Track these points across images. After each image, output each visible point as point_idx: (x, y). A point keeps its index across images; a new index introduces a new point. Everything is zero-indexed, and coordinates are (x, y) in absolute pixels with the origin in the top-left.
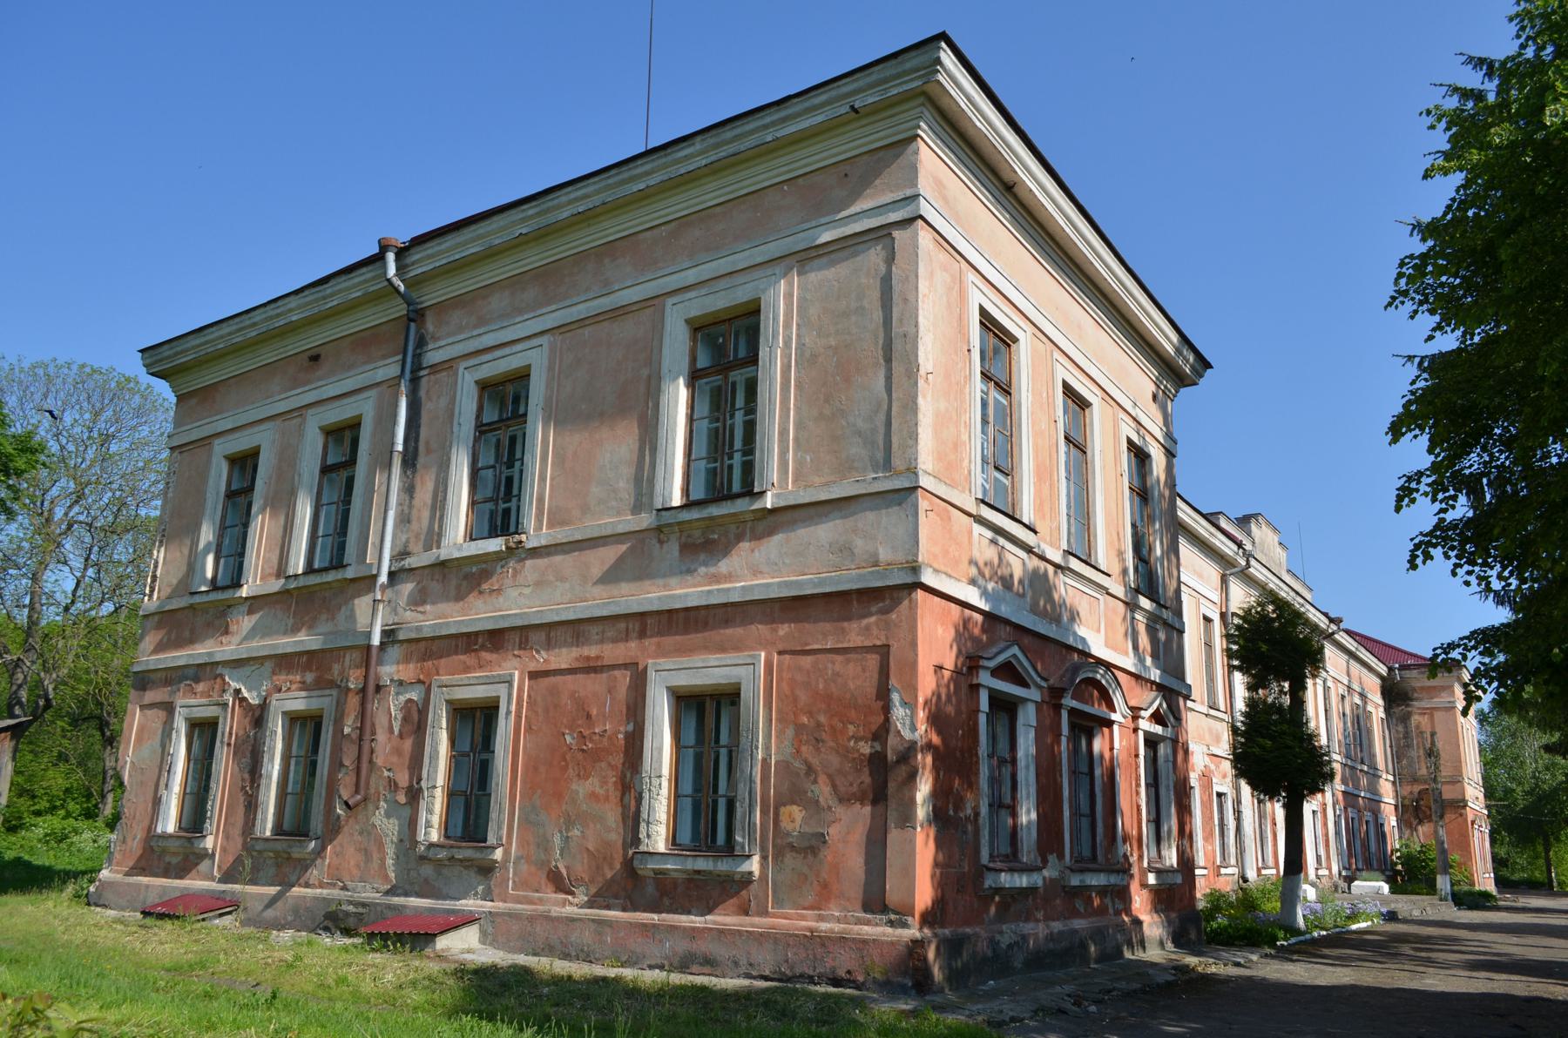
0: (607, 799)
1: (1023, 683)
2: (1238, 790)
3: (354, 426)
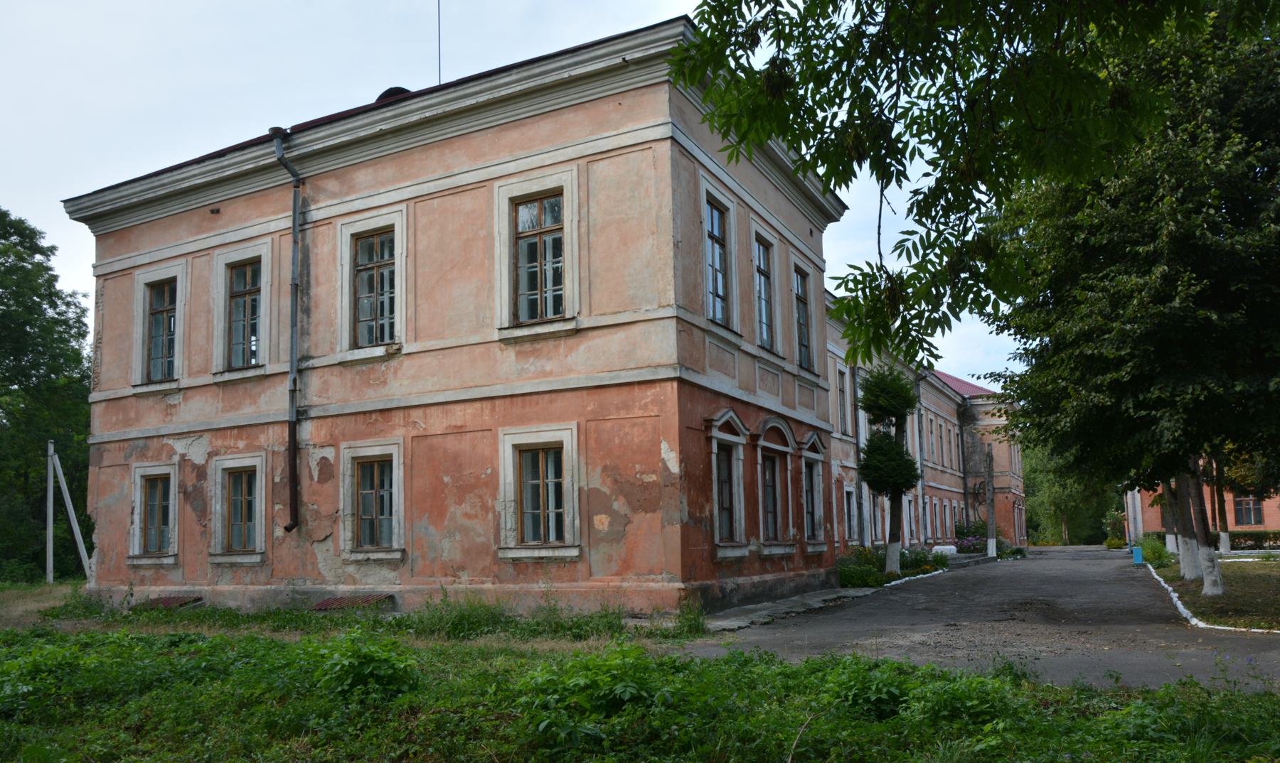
0: (476, 516)
1: (736, 433)
2: (859, 489)
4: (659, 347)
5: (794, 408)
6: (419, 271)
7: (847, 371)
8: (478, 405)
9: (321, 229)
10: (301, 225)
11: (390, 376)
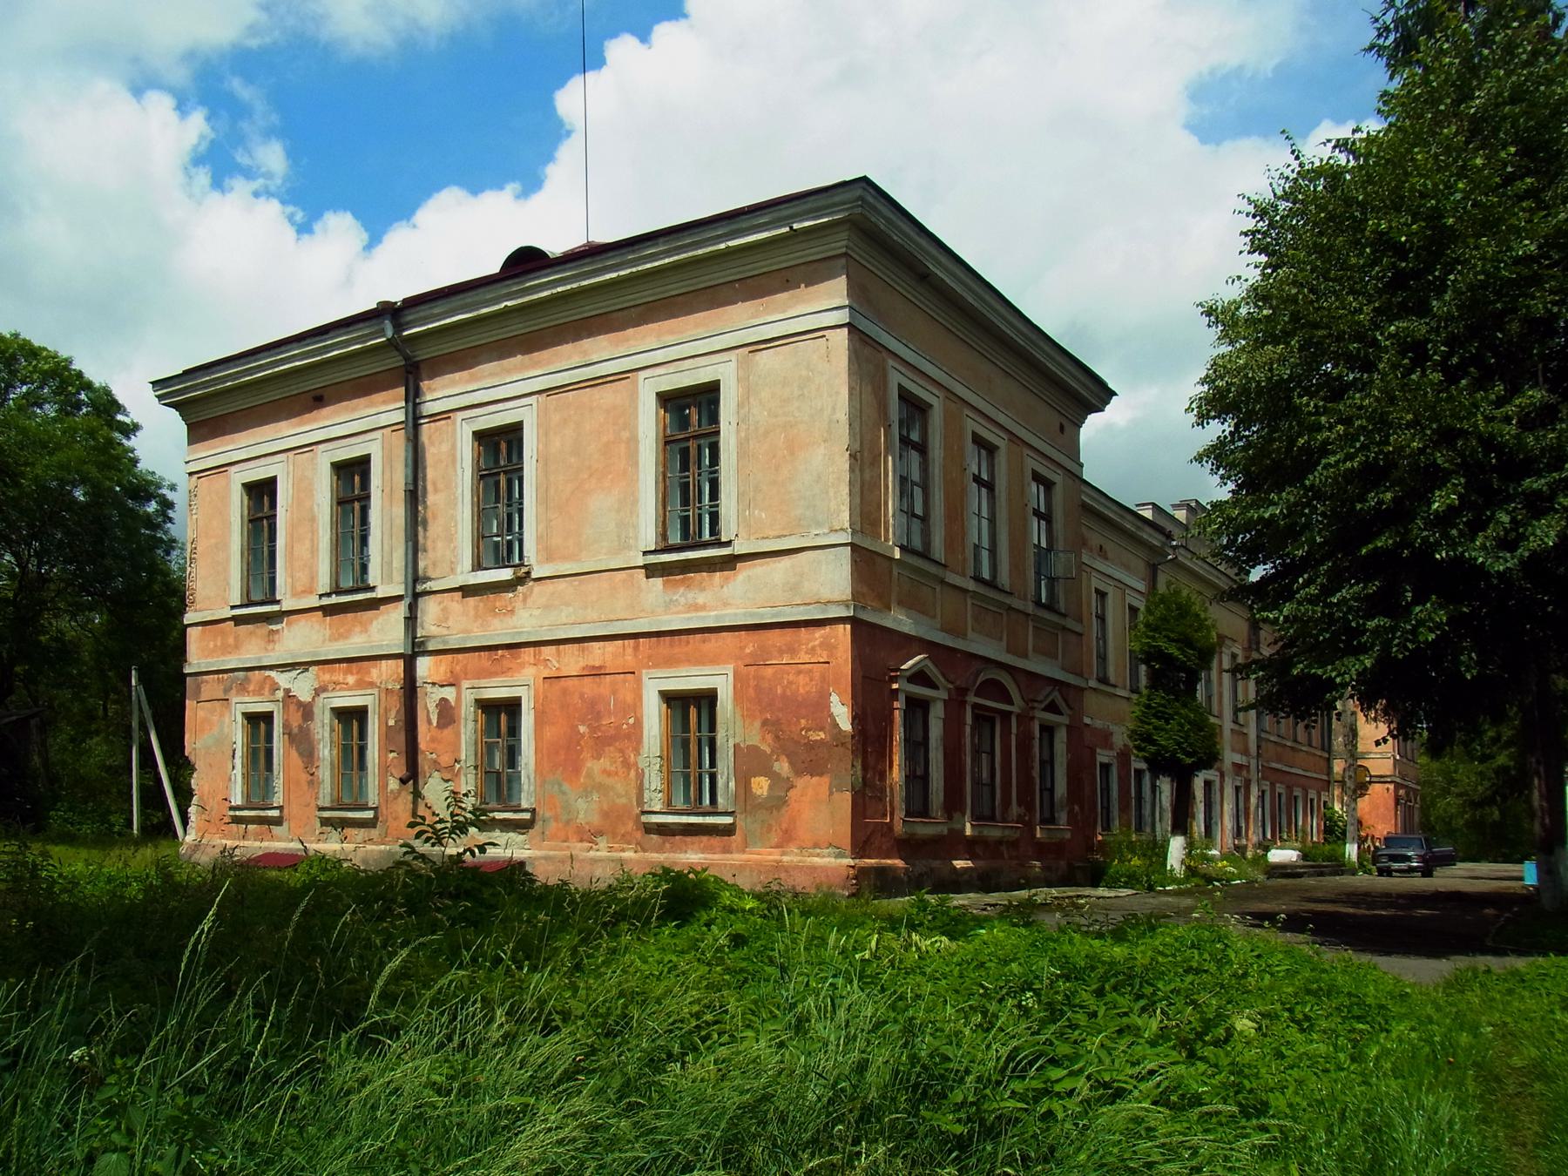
1: (934, 686)
3: (362, 464)
4: (830, 581)
11: (518, 604)
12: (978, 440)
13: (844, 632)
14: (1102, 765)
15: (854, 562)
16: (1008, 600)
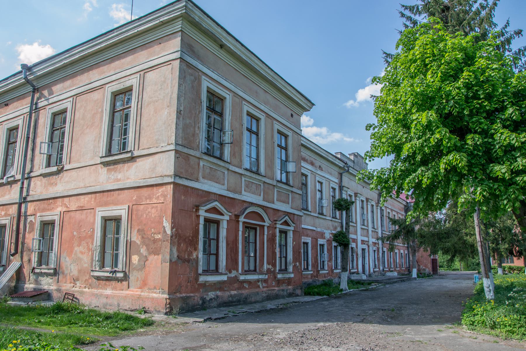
1: (222, 214)
4: (165, 166)
5: (273, 203)
6: (74, 129)
7: (337, 188)
8: (90, 196)
9: (41, 111)
10: (35, 109)
11: (58, 181)
12: (279, 132)
13: (170, 188)
14: (320, 245)
15: (176, 158)
16: (264, 179)
